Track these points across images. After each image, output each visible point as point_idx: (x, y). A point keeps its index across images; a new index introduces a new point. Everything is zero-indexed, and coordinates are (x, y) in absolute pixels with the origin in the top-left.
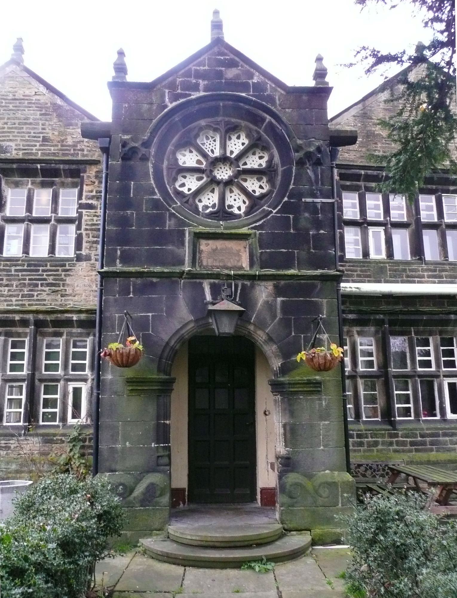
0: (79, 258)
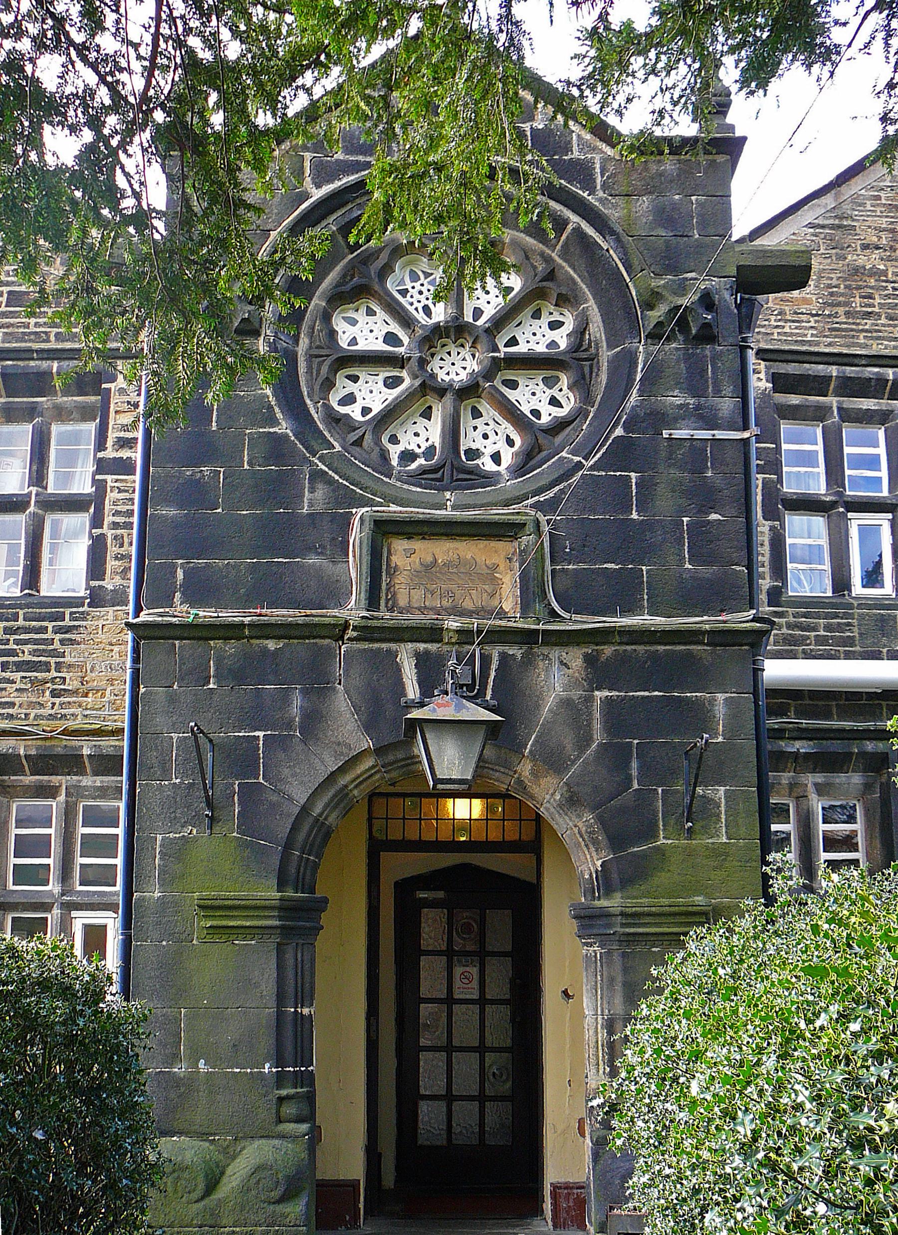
0: (97, 598)
